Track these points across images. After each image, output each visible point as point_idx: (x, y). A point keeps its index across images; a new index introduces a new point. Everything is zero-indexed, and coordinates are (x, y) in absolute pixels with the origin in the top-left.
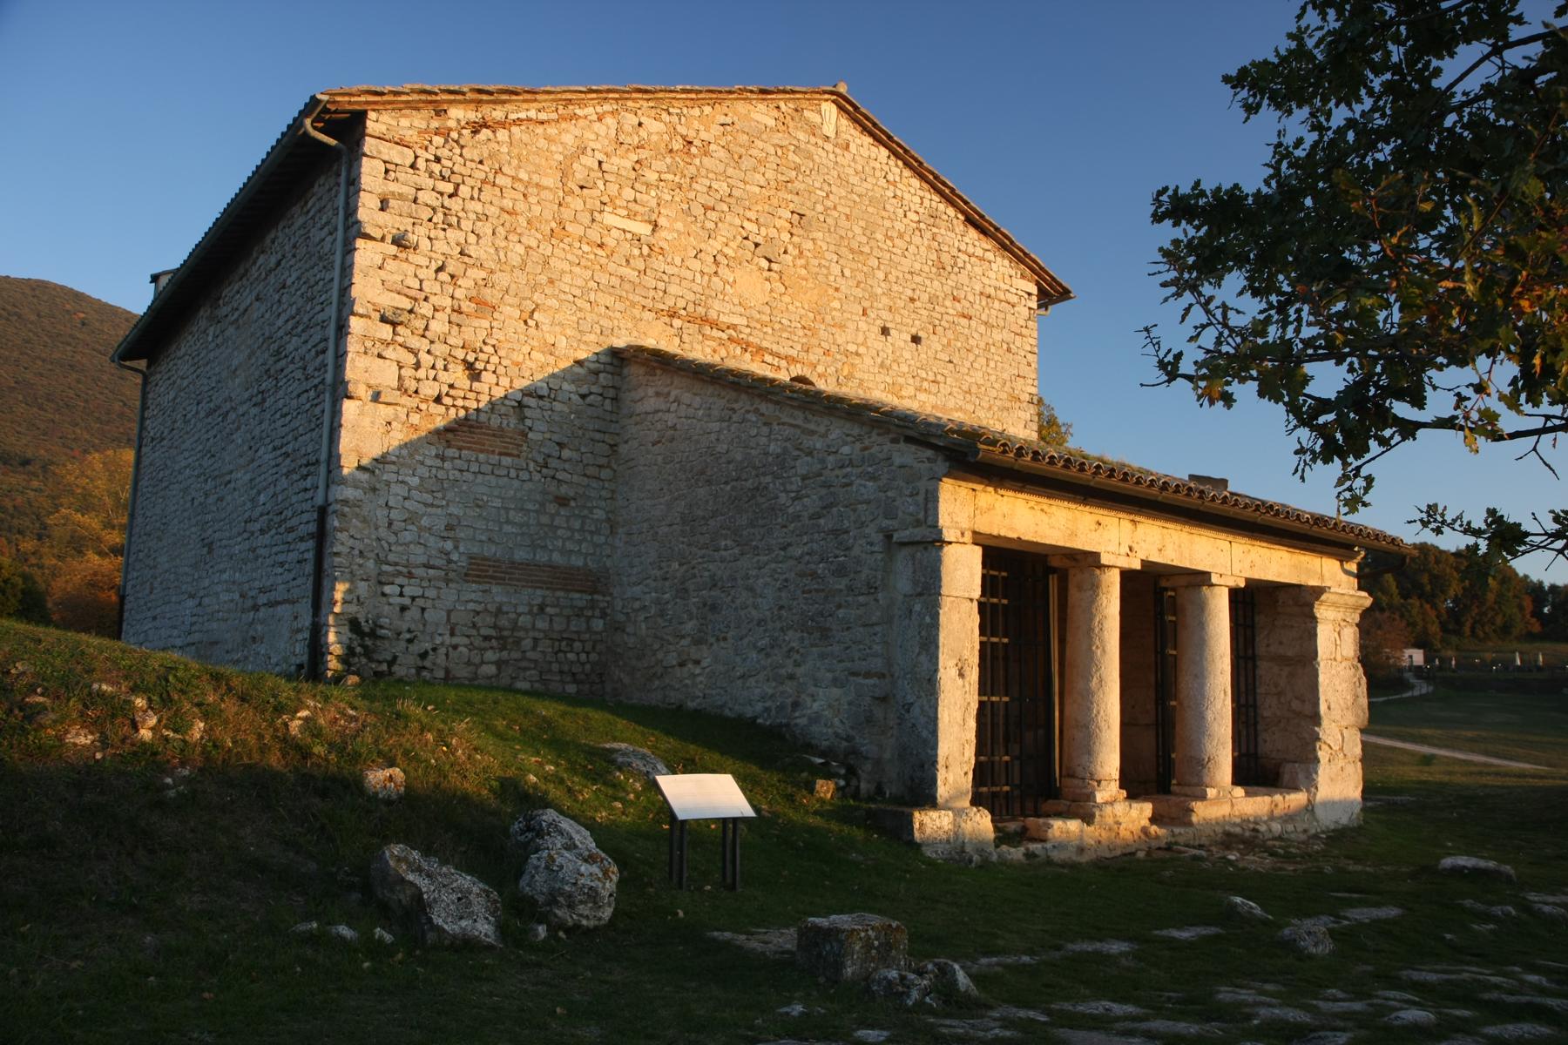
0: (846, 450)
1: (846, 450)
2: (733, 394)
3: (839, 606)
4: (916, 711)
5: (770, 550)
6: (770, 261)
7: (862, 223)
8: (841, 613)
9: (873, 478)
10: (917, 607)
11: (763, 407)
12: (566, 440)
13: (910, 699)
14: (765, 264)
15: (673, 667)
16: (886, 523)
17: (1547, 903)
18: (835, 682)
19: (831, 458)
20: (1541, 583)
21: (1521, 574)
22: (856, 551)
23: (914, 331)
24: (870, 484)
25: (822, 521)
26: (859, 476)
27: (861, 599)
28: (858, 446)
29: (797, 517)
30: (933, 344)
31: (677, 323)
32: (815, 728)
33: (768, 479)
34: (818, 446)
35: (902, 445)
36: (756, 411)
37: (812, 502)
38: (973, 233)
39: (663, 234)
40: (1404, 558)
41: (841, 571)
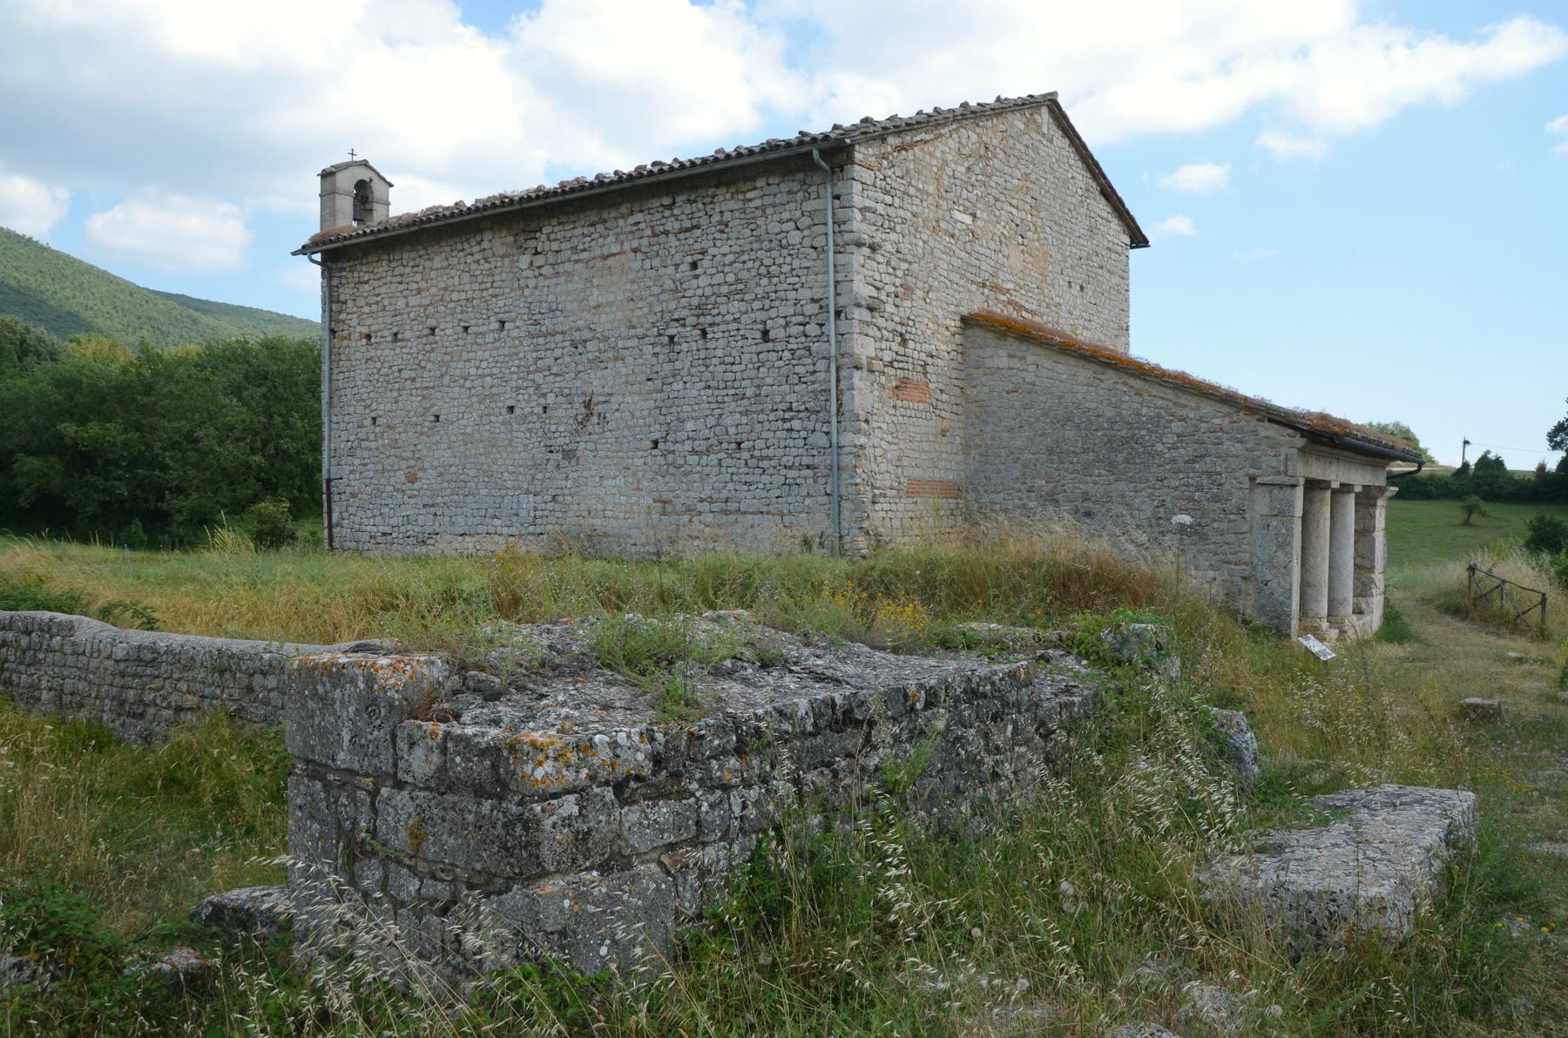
0: (1217, 421)
1: (1217, 421)
2: (1099, 369)
3: (1214, 520)
4: (1273, 585)
5: (1148, 481)
8: (1216, 525)
9: (1241, 442)
10: (1274, 523)
11: (1132, 381)
14: (1020, 240)
15: (1494, 565)
16: (1252, 471)
18: (1212, 567)
19: (1204, 425)
22: (1227, 486)
25: (1197, 466)
27: (1232, 517)
28: (1227, 420)
29: (1173, 461)
30: (1089, 290)
31: (986, 291)
33: (1143, 432)
34: (1191, 415)
35: (1266, 424)
36: (1125, 384)
37: (1186, 452)
38: (1103, 201)
39: (979, 223)
40: (1446, 484)
41: (1215, 498)
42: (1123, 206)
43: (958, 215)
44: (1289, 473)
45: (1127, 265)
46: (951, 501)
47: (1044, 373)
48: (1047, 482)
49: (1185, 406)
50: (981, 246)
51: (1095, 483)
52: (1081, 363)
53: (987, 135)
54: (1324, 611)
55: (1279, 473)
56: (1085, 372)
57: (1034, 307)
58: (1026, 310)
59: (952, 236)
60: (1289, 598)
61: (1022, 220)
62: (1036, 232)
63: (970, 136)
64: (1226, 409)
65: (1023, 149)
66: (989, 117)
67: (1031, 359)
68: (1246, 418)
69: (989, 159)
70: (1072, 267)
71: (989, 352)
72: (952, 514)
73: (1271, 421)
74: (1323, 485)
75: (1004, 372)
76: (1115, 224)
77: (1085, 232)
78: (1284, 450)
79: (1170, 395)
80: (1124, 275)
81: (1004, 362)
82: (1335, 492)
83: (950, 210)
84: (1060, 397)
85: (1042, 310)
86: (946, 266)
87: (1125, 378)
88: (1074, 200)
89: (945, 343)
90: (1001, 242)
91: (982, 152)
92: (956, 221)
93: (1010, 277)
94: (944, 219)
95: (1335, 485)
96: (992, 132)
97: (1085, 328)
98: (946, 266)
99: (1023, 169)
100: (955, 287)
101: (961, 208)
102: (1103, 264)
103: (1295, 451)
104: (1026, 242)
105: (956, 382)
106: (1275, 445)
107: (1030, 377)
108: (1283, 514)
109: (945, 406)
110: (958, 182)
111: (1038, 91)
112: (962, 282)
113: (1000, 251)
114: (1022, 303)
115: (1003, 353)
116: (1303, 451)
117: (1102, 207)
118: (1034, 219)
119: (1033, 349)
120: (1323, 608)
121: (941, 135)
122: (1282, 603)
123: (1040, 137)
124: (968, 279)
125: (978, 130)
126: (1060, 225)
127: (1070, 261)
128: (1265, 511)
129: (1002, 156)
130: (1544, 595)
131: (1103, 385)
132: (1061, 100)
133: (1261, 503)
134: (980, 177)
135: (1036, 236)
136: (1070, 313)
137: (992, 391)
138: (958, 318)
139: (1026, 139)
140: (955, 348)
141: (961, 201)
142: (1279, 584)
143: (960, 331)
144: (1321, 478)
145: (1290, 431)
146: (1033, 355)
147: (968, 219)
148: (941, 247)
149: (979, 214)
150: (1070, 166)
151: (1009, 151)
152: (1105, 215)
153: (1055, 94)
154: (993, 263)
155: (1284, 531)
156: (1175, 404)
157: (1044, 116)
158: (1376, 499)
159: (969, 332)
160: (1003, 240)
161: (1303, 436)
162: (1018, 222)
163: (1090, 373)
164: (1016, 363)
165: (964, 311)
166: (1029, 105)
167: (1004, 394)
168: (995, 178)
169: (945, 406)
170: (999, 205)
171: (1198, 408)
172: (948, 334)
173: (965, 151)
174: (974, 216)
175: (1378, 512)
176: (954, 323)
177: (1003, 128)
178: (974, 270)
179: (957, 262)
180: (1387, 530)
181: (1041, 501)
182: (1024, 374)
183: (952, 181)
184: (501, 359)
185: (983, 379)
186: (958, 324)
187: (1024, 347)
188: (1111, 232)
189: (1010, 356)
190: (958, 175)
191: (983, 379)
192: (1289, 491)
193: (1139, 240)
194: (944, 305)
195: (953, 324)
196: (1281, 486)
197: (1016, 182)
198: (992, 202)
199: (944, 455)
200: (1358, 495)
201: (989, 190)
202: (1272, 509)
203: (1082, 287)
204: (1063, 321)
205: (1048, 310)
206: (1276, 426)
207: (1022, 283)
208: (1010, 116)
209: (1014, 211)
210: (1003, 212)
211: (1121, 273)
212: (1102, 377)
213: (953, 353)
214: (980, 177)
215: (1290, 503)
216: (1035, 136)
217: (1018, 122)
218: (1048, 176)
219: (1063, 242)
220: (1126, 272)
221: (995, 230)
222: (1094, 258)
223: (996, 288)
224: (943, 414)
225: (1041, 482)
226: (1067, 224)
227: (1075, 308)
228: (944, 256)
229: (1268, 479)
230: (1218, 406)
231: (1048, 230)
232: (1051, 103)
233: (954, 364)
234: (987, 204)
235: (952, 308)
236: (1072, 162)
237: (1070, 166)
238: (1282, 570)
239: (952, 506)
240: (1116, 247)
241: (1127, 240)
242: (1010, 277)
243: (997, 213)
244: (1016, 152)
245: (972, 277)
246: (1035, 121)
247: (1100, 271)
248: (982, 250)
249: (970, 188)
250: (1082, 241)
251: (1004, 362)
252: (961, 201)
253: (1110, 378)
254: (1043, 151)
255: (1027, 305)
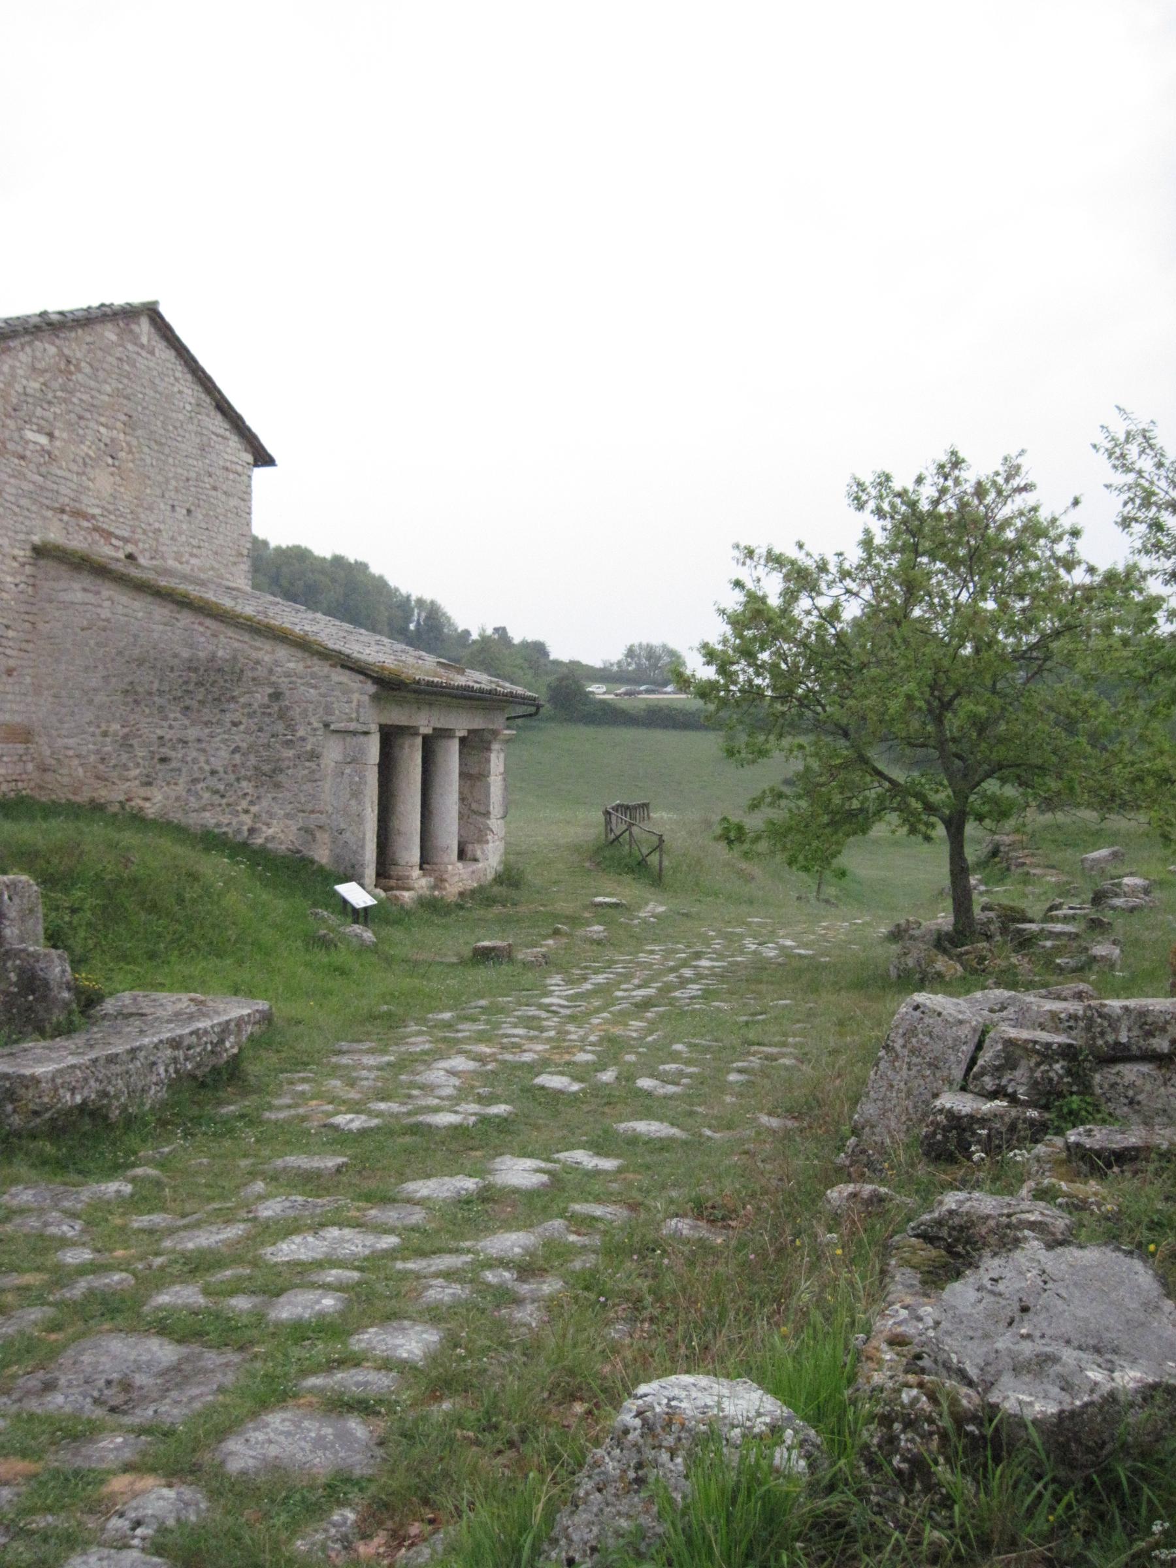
6: (113, 458)
7: (161, 418)
9: (315, 687)
10: (348, 771)
12: (9, 623)
13: (343, 826)
14: (110, 461)
17: (5, 1399)
19: (279, 669)
20: (408, 597)
21: (352, 561)
23: (188, 505)
24: (312, 691)
26: (303, 684)
31: (65, 517)
32: (270, 846)
34: (266, 658)
35: (339, 669)
36: (200, 624)
38: (219, 417)
39: (58, 443)
41: (288, 744)
42: (243, 422)
43: (30, 435)
44: (361, 720)
45: (249, 486)
46: (18, 746)
47: (120, 609)
48: (123, 726)
49: (261, 649)
50: (60, 468)
51: (171, 727)
52: (158, 600)
53: (69, 347)
54: (415, 856)
55: (351, 720)
56: (161, 611)
57: (126, 534)
58: (117, 537)
59: (23, 457)
60: (363, 847)
61: (113, 440)
62: (130, 452)
63: (47, 350)
64: (299, 654)
65: (115, 362)
66: (72, 329)
67: (105, 593)
68: (319, 662)
69: (71, 373)
70: (177, 490)
71: (62, 585)
72: (20, 760)
73: (343, 666)
74: (412, 731)
75: (77, 607)
76: (234, 441)
77: (194, 451)
78: (355, 697)
79: (246, 637)
80: (245, 496)
81: (79, 596)
82: (426, 739)
83: (20, 429)
84: (135, 636)
85: (137, 536)
86: (13, 491)
87: (201, 619)
88: (181, 417)
89: (13, 575)
90: (85, 464)
91: (63, 366)
92: (27, 442)
93: (96, 502)
94: (11, 439)
95: (427, 730)
96: (76, 346)
97: (192, 555)
98: (13, 491)
99: (115, 384)
100: (27, 513)
101: (35, 427)
102: (218, 484)
103: (367, 698)
104: (117, 463)
105: (26, 617)
106: (347, 691)
107: (105, 613)
108: (355, 759)
109: (11, 644)
110: (30, 400)
111: (137, 298)
112: (34, 508)
113: (84, 473)
114: (112, 529)
115: (76, 586)
116: (375, 698)
117: (217, 423)
118: (128, 438)
119: (108, 584)
120: (413, 855)
121: (9, 349)
122: (355, 852)
123: (136, 349)
124: (42, 505)
125: (57, 342)
126: (161, 444)
127: (173, 483)
128: (339, 758)
129: (88, 370)
130: (661, 836)
131: (178, 624)
132: (162, 309)
133: (333, 752)
134: (59, 394)
135: (130, 457)
136: (172, 538)
137: (65, 627)
138: (28, 547)
139: (118, 352)
140: (23, 579)
141: (34, 420)
142: (353, 833)
143: (32, 561)
144: (406, 724)
145: (361, 677)
146: (108, 591)
147: (43, 440)
148: (8, 470)
149: (57, 433)
150: (176, 379)
151: (96, 364)
152: (221, 431)
153: (156, 303)
154: (75, 487)
155: (357, 779)
156: (251, 647)
157: (144, 327)
158: (490, 742)
159: (42, 562)
160: (85, 462)
161: (374, 683)
162: (108, 441)
163: (166, 612)
164: (90, 598)
165: (36, 539)
166: (127, 315)
167: (78, 630)
168: (78, 394)
169: (11, 644)
170: (82, 423)
171: (273, 652)
172: (15, 564)
173: (40, 365)
174: (51, 435)
175: (493, 756)
176: (23, 553)
177: (89, 339)
178: (50, 495)
179: (27, 486)
180: (506, 774)
181: (116, 746)
182: (99, 610)
183: (23, 398)
184: (179, 439)
185: (57, 614)
186: (29, 553)
187: (99, 582)
188: (229, 450)
189: (85, 590)
190: (29, 391)
191: (57, 614)
192: (362, 739)
193: (263, 458)
194: (10, 534)
195: (22, 553)
196: (354, 733)
197: (106, 398)
198: (73, 417)
199: (10, 697)
200: (463, 740)
201: (71, 407)
202: (345, 757)
203: (189, 511)
204: (164, 549)
205: (143, 537)
206: (348, 672)
207: (111, 507)
208: (99, 328)
209: (102, 430)
210: (89, 432)
211: (240, 495)
212: (178, 616)
213: (22, 586)
214: (59, 394)
215: (363, 751)
216: (130, 347)
217: (109, 333)
218: (147, 391)
219: (165, 462)
220: (249, 494)
221: (78, 451)
222: (206, 479)
223: (78, 514)
224: (8, 651)
225: (115, 727)
226: (169, 442)
227: (180, 534)
228: (12, 481)
229: (341, 726)
230: (293, 651)
231: (146, 450)
232: (152, 312)
233: (23, 597)
234: (69, 424)
235: (22, 537)
236: (178, 375)
237: (176, 379)
238: (356, 819)
239: (21, 752)
240: (234, 467)
241: (250, 458)
242: (96, 502)
243: (81, 432)
244: (105, 366)
245: (47, 502)
246: (131, 331)
247: (213, 493)
248: (59, 472)
249: (46, 406)
250: (190, 461)
251: (79, 596)
252: (34, 420)
253: (186, 618)
254: (141, 363)
255: (118, 532)
